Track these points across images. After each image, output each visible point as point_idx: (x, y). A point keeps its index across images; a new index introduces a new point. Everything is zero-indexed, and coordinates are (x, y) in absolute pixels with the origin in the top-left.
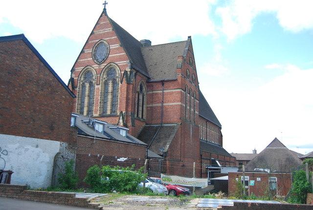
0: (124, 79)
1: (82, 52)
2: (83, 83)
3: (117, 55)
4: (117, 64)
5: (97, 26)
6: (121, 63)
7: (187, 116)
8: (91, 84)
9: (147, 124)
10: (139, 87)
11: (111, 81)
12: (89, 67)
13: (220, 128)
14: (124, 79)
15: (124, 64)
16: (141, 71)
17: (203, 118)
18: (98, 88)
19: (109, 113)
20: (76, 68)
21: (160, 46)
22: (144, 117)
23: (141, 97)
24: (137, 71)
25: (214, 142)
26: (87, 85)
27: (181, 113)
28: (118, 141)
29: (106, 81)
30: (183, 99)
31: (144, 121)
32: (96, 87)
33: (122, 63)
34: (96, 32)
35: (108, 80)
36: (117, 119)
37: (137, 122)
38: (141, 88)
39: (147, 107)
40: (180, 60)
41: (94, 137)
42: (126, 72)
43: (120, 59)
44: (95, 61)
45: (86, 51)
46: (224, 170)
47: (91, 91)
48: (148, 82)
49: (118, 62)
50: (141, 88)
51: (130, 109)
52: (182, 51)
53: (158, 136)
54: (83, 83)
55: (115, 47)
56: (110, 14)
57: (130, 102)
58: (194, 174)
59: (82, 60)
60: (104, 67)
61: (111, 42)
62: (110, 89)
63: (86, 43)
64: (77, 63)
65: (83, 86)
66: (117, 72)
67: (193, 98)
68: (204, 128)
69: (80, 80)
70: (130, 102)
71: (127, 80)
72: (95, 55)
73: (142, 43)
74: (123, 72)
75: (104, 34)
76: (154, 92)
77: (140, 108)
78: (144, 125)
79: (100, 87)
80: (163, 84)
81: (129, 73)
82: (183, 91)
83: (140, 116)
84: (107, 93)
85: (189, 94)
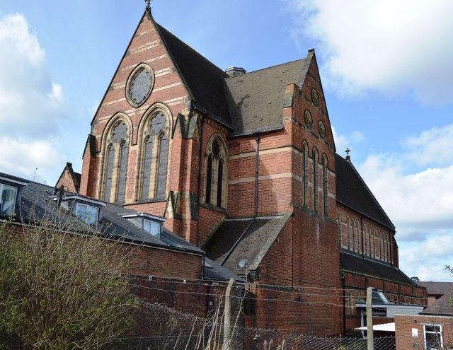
2: (111, 145)
4: (166, 105)
6: (173, 102)
7: (307, 201)
9: (227, 218)
10: (211, 145)
12: (120, 114)
13: (394, 232)
14: (178, 124)
15: (179, 103)
20: (99, 119)
21: (257, 73)
22: (224, 204)
23: (215, 165)
25: (380, 257)
29: (148, 137)
31: (223, 212)
32: (132, 148)
35: (153, 133)
39: (229, 186)
42: (181, 117)
43: (173, 94)
44: (131, 102)
46: (393, 311)
48: (229, 138)
49: (169, 101)
52: (299, 77)
54: (111, 145)
58: (429, 332)
59: (109, 103)
60: (143, 112)
66: (167, 119)
67: (320, 166)
68: (357, 230)
72: (130, 94)
73: (228, 73)
74: (175, 118)
75: (146, 52)
76: (241, 156)
77: (215, 187)
78: (223, 219)
79: (136, 148)
80: (258, 141)
81: (187, 118)
83: (214, 201)
85: (313, 158)
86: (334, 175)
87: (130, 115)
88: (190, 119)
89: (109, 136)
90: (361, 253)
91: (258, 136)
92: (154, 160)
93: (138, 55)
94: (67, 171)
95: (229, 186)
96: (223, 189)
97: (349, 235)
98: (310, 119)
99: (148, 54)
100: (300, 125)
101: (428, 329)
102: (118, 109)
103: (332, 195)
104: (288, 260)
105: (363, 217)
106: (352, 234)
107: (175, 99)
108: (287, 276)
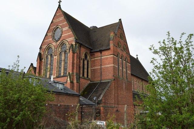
0: (71, 50)
1: (46, 35)
3: (67, 34)
5: (55, 17)
6: (69, 40)
7: (120, 74)
8: (51, 55)
9: (91, 82)
11: (63, 53)
14: (71, 50)
15: (71, 40)
16: (84, 44)
17: (146, 80)
19: (62, 74)
22: (89, 77)
23: (86, 62)
27: (114, 72)
31: (89, 80)
32: (55, 57)
33: (70, 39)
35: (62, 52)
37: (82, 81)
39: (91, 70)
42: (72, 45)
43: (69, 36)
44: (54, 40)
45: (49, 34)
47: (51, 61)
48: (91, 52)
49: (68, 39)
51: (75, 71)
54: (47, 56)
55: (66, 29)
56: (63, 8)
57: (75, 65)
60: (58, 43)
62: (63, 58)
63: (49, 29)
64: (44, 43)
69: (45, 54)
70: (75, 65)
71: (73, 51)
72: (54, 37)
73: (91, 28)
75: (59, 21)
76: (95, 59)
77: (86, 70)
78: (89, 82)
79: (56, 57)
80: (101, 53)
81: (74, 45)
82: (115, 56)
83: (86, 76)
85: (122, 58)
86: (130, 64)
87: (54, 45)
88: (75, 46)
89: (46, 53)
91: (101, 51)
92: (63, 61)
93: (56, 22)
94: (31, 67)
95: (91, 70)
96: (89, 71)
97: (137, 86)
99: (60, 22)
100: (116, 47)
102: (49, 43)
103: (129, 72)
104: (113, 96)
107: (70, 39)
108: (112, 103)
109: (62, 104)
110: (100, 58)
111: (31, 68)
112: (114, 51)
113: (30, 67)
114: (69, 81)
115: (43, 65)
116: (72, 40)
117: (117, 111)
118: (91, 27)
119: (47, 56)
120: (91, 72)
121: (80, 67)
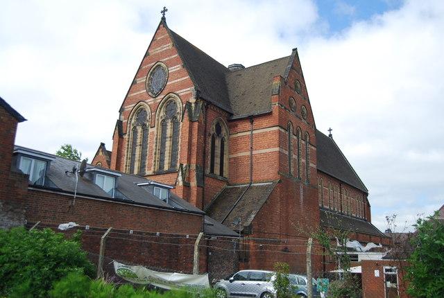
0: (186, 114)
1: (134, 82)
3: (179, 80)
4: (177, 95)
6: (182, 92)
7: (292, 170)
8: (144, 126)
11: (170, 121)
14: (186, 114)
15: (187, 93)
17: (331, 176)
18: (153, 132)
19: (166, 168)
22: (225, 174)
23: (218, 143)
24: (209, 103)
26: (139, 129)
28: (134, 203)
30: (283, 141)
33: (184, 90)
34: (152, 52)
35: (167, 118)
36: (175, 175)
37: (209, 182)
38: (219, 130)
40: (277, 83)
41: (74, 193)
42: (189, 104)
43: (183, 86)
44: (150, 93)
48: (230, 121)
49: (179, 91)
50: (219, 130)
53: (241, 202)
54: (135, 127)
56: (171, 25)
61: (169, 64)
62: (169, 132)
65: (135, 132)
66: (178, 106)
70: (195, 148)
74: (184, 105)
75: (161, 53)
76: (239, 135)
77: (217, 160)
79: (154, 130)
80: (252, 123)
81: (193, 105)
82: (283, 131)
83: (217, 172)
84: (165, 138)
86: (315, 149)
87: (149, 103)
89: (133, 121)
90: (340, 211)
91: (251, 119)
95: (230, 159)
98: (294, 104)
100: (285, 108)
101: (387, 270)
105: (341, 183)
106: (331, 197)
107: (184, 90)
108: (275, 231)
109: (165, 232)
110: (249, 133)
111: (101, 154)
112: (280, 119)
113: (98, 151)
114: (181, 183)
115: (126, 146)
116: (189, 92)
117: (286, 250)
118: (230, 66)
119: (135, 127)
120: (230, 163)
121: (204, 153)
